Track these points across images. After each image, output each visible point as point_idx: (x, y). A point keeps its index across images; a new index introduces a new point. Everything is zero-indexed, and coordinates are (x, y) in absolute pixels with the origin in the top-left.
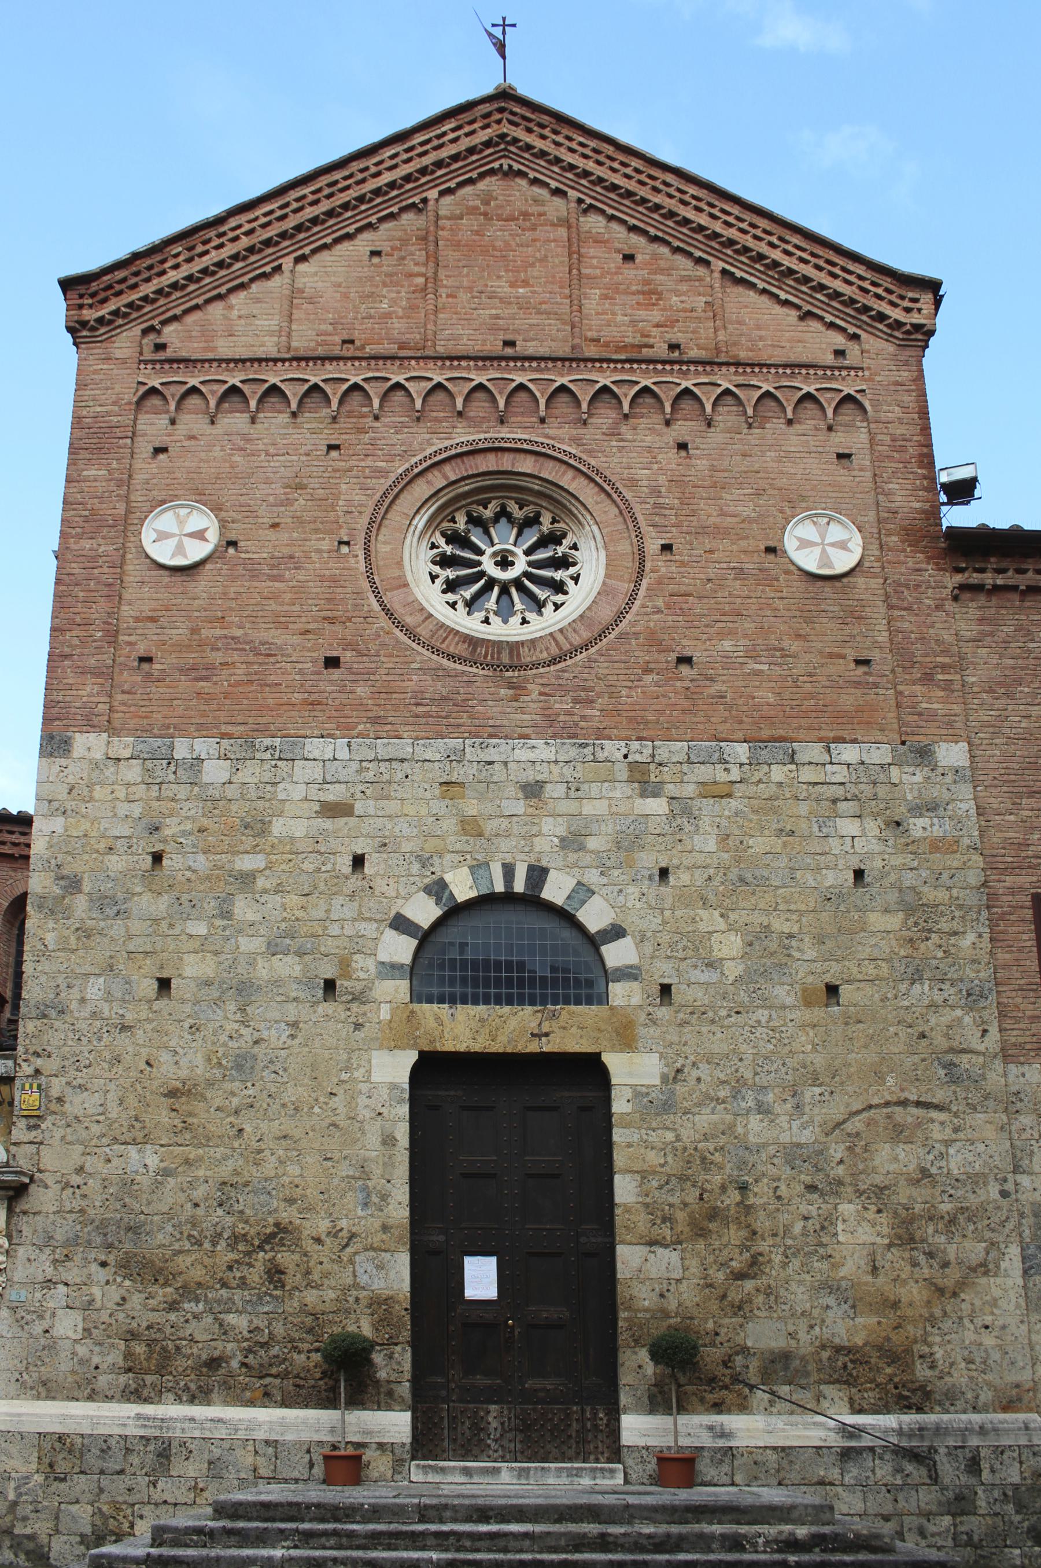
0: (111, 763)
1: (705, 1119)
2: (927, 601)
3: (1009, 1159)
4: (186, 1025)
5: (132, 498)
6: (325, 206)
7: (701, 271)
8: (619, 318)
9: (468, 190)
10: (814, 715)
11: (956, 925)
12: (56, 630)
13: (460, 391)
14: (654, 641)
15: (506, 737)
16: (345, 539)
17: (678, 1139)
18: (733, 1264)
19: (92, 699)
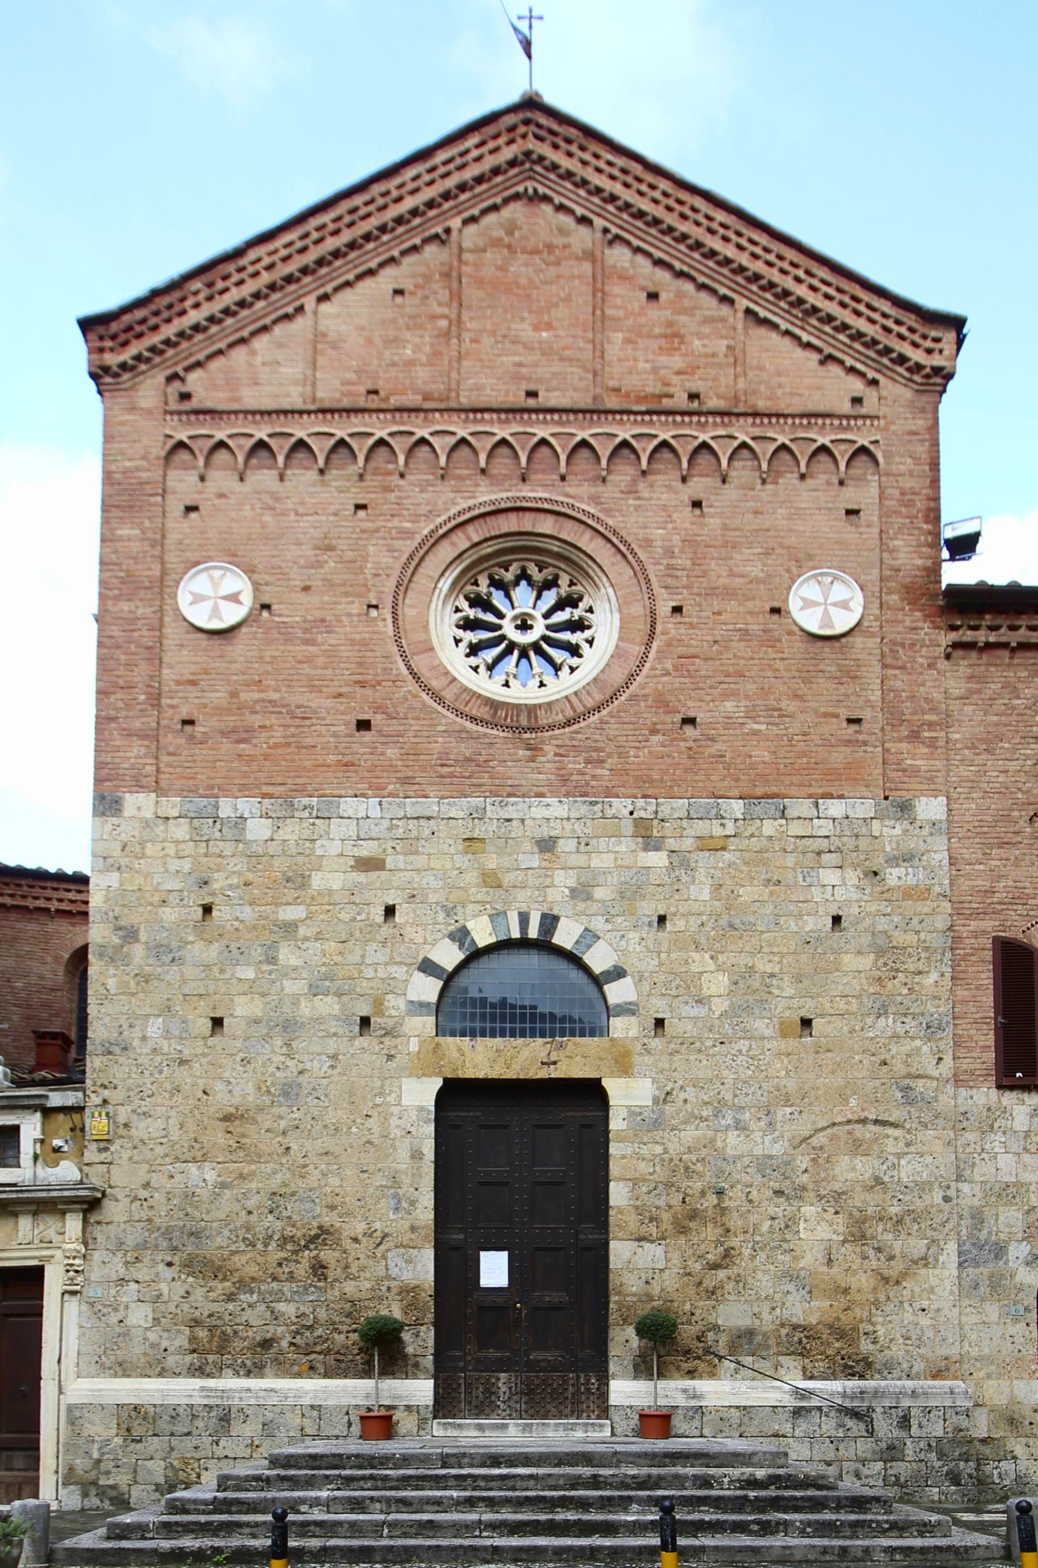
0: (160, 822)
1: (690, 1134)
2: (920, 660)
3: (953, 1169)
4: (238, 1059)
5: (167, 559)
6: (346, 236)
7: (725, 310)
8: (641, 365)
9: (492, 218)
10: (805, 772)
11: (921, 966)
12: (101, 693)
13: (483, 446)
14: (662, 703)
15: (524, 796)
16: (374, 603)
17: (666, 1151)
18: (709, 1256)
19: (140, 761)
